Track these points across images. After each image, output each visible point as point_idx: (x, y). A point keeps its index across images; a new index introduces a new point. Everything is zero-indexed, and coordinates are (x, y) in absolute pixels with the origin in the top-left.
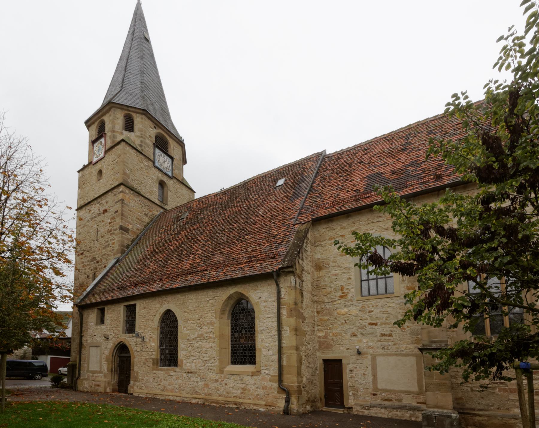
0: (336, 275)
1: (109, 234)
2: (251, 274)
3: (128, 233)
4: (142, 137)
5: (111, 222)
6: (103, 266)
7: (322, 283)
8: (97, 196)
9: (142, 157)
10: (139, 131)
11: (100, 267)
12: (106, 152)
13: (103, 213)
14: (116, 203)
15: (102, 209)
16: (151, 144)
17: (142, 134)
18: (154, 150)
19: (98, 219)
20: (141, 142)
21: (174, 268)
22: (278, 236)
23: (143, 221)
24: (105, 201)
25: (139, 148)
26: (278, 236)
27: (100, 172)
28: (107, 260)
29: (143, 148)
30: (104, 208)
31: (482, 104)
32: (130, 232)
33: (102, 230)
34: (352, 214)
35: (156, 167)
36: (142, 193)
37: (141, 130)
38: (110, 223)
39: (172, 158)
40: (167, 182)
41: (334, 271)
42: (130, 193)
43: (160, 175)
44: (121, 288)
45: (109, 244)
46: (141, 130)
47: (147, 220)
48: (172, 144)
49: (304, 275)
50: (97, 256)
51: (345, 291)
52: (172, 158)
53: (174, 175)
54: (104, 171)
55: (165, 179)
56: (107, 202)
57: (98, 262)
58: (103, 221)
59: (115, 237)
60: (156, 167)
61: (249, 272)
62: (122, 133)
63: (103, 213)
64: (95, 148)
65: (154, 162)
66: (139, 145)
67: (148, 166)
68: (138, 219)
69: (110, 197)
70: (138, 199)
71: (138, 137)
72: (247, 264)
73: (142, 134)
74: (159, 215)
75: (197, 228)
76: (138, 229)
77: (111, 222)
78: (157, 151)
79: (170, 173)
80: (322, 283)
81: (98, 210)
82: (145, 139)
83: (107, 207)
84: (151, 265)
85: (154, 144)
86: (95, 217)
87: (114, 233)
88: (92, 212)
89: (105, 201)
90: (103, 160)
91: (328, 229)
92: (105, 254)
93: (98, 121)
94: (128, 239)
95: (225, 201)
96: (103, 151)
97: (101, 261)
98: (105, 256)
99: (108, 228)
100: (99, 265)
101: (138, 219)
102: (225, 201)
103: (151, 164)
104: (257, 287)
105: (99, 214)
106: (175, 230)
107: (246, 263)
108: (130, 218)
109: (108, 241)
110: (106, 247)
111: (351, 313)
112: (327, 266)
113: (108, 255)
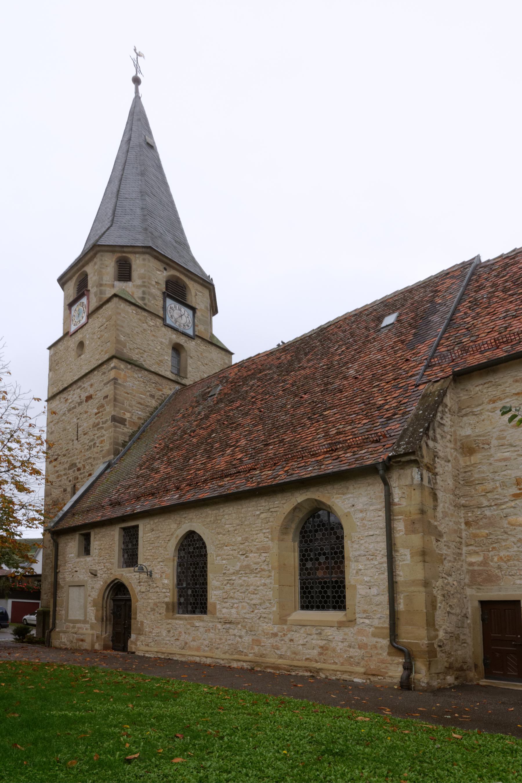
1: (96, 429)
3: (125, 425)
4: (145, 286)
6: (87, 474)
11: (82, 476)
12: (89, 316)
13: (86, 401)
15: (84, 396)
16: (159, 294)
17: (144, 282)
19: (79, 409)
20: (144, 293)
23: (147, 406)
25: (140, 303)
27: (81, 345)
28: (92, 465)
30: (87, 394)
32: (127, 423)
33: (85, 425)
37: (142, 277)
38: (96, 414)
39: (194, 309)
40: (185, 345)
42: (126, 368)
43: (174, 336)
45: (95, 443)
46: (142, 277)
47: (154, 403)
48: (193, 287)
49: (438, 465)
50: (77, 461)
52: (194, 309)
53: (197, 333)
54: (87, 343)
55: (182, 340)
57: (79, 469)
58: (86, 412)
59: (104, 432)
62: (113, 286)
63: (86, 401)
64: (73, 312)
65: (164, 319)
66: (139, 298)
67: (155, 326)
69: (96, 377)
70: (140, 375)
73: (144, 282)
77: (99, 413)
78: (169, 302)
79: (190, 332)
81: (78, 398)
83: (91, 391)
85: (164, 293)
86: (74, 408)
87: (102, 428)
88: (70, 401)
89: (89, 383)
91: (486, 386)
92: (90, 458)
94: (124, 434)
96: (85, 316)
97: (84, 467)
98: (89, 461)
99: (94, 420)
100: (81, 474)
103: (159, 322)
105: (80, 404)
109: (93, 440)
110: (90, 447)
112: (486, 446)
113: (94, 458)
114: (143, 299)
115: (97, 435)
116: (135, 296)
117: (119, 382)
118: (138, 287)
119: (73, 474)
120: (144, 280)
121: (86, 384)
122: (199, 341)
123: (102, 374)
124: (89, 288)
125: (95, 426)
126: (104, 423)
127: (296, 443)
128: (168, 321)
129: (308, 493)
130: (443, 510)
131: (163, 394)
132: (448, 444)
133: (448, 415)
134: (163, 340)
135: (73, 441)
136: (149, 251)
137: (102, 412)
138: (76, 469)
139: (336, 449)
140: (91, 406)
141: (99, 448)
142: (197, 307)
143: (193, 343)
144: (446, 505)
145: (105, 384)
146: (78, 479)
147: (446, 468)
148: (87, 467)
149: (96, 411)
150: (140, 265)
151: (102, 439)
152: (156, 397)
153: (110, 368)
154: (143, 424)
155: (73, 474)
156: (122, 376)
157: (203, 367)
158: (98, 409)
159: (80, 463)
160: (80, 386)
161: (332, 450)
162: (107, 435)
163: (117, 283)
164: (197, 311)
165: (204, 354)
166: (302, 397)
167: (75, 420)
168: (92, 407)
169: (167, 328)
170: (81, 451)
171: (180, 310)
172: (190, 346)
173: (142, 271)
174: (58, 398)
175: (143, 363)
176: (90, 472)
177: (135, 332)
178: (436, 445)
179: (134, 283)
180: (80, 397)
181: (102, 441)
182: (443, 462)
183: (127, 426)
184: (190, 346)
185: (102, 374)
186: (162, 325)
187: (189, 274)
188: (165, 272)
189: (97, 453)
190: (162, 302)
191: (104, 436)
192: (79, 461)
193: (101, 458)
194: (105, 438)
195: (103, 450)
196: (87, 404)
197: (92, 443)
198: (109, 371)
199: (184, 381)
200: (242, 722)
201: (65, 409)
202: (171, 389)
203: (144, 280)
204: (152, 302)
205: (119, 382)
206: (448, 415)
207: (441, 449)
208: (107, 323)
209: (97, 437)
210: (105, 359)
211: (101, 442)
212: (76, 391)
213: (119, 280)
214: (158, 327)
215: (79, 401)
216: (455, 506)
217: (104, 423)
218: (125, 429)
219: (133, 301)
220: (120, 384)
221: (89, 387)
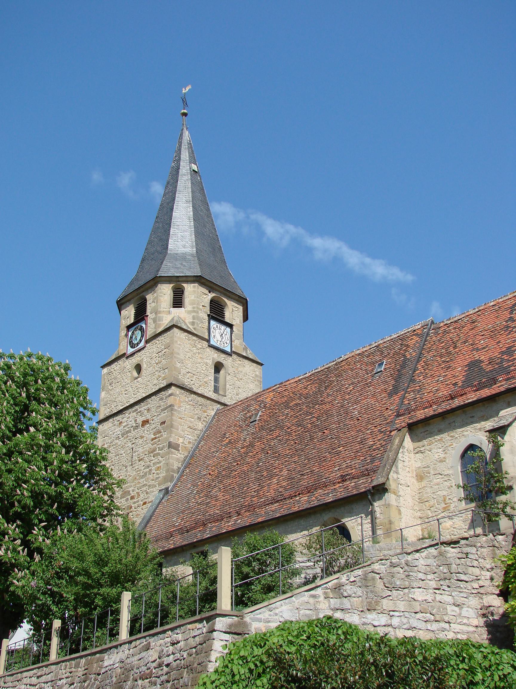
0: (438, 484)
1: (152, 455)
2: (345, 496)
3: (179, 450)
4: (194, 312)
5: (156, 438)
6: (142, 503)
7: (425, 495)
8: (132, 401)
9: (194, 338)
10: (190, 304)
11: (136, 505)
13: (143, 425)
14: (162, 410)
15: (140, 420)
17: (194, 308)
18: (209, 323)
19: (133, 433)
20: (194, 318)
21: (253, 497)
22: (374, 447)
23: (195, 430)
24: (146, 407)
25: (191, 328)
26: (374, 447)
27: (138, 368)
28: (147, 493)
29: (195, 326)
30: (144, 418)
31: (236, 594)
32: (180, 449)
33: (141, 450)
34: (446, 416)
35: (211, 346)
36: (195, 390)
37: (192, 303)
38: (153, 440)
39: (230, 326)
40: (224, 362)
41: (435, 480)
43: (216, 356)
44: (182, 531)
45: (151, 470)
46: (192, 303)
47: (200, 426)
49: (401, 490)
50: (131, 489)
51: (447, 501)
52: (230, 326)
53: (233, 349)
54: (144, 366)
55: (221, 358)
56: (148, 410)
57: (132, 498)
58: (142, 437)
59: (161, 459)
60: (211, 346)
61: (341, 494)
62: (169, 312)
63: (143, 425)
65: (208, 341)
66: (189, 323)
68: (189, 427)
69: (154, 402)
71: (189, 312)
72: (341, 485)
73: (194, 308)
74: (215, 414)
75: (277, 437)
76: (189, 442)
77: (156, 438)
78: (213, 323)
79: (228, 349)
80: (425, 495)
81: (133, 422)
82: (198, 312)
83: (149, 417)
84: (220, 495)
85: (209, 315)
86: (129, 431)
87: (158, 454)
88: (124, 425)
89: (146, 407)
90: (143, 352)
91: (426, 433)
92: (145, 485)
93: (136, 298)
94: (178, 460)
95: (311, 392)
97: (139, 495)
98: (144, 488)
99: (149, 446)
100: (134, 503)
101: (189, 427)
102: (311, 392)
103: (205, 344)
104: (353, 509)
106: (245, 440)
107: (339, 483)
108: (180, 428)
109: (148, 467)
110: (146, 474)
111: (456, 526)
112: (428, 475)
113: (149, 486)
114: (193, 323)
115: (153, 462)
116: (187, 321)
117: (176, 408)
118: (189, 312)
119: (126, 503)
120: (194, 306)
121: (142, 407)
122: (234, 356)
123: (160, 400)
124: (148, 313)
125: (152, 452)
126: (161, 449)
127: (321, 474)
128: (212, 342)
129: (330, 514)
130: (406, 521)
131: (208, 416)
132: (408, 474)
133: (406, 454)
134: (208, 361)
135: (126, 467)
136: (199, 280)
137: (158, 437)
138: (129, 497)
139: (346, 480)
140: (147, 431)
141: (155, 475)
142: (233, 324)
143: (230, 359)
144: (408, 517)
145: (162, 410)
146: (131, 508)
147: (407, 491)
148: (142, 496)
149: (153, 436)
150: (191, 291)
151: (158, 465)
152: (202, 420)
153: (167, 394)
154: (192, 448)
155: (126, 503)
156: (177, 402)
157: (239, 383)
158: (154, 434)
159: (133, 491)
160: (137, 410)
161: (343, 481)
162: (164, 462)
163: (172, 309)
164: (234, 327)
165: (240, 369)
166: (324, 433)
167: (130, 444)
168: (148, 433)
169: (210, 348)
170: (136, 478)
171: (220, 329)
172: (227, 361)
173: (193, 298)
174: (111, 420)
175: (193, 386)
176: (144, 501)
177: (187, 357)
178: (399, 476)
179: (186, 309)
180: (136, 420)
181: (158, 467)
182: (404, 488)
183: (180, 452)
184: (227, 361)
185: (160, 400)
186: (207, 346)
187: (228, 293)
188: (209, 294)
189: (153, 480)
190: (207, 323)
191: (160, 462)
192: (132, 488)
193: (157, 485)
194: (161, 464)
195: (159, 477)
196: (143, 429)
197: (148, 470)
198: (166, 397)
199: (223, 400)
200: (317, 553)
201: (119, 432)
202: (213, 410)
203: (194, 306)
204: (200, 325)
205: (176, 408)
206: (406, 454)
207: (402, 478)
208: (165, 350)
209: (154, 464)
210: (162, 386)
211: (158, 468)
212: (131, 414)
213: (174, 307)
214: (204, 349)
215: (134, 425)
216: (414, 518)
217: (161, 449)
218: (178, 454)
219: (185, 327)
220: (176, 410)
221: (146, 411)
